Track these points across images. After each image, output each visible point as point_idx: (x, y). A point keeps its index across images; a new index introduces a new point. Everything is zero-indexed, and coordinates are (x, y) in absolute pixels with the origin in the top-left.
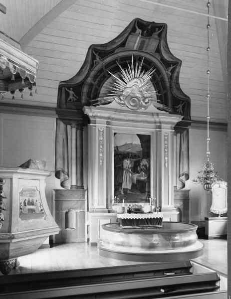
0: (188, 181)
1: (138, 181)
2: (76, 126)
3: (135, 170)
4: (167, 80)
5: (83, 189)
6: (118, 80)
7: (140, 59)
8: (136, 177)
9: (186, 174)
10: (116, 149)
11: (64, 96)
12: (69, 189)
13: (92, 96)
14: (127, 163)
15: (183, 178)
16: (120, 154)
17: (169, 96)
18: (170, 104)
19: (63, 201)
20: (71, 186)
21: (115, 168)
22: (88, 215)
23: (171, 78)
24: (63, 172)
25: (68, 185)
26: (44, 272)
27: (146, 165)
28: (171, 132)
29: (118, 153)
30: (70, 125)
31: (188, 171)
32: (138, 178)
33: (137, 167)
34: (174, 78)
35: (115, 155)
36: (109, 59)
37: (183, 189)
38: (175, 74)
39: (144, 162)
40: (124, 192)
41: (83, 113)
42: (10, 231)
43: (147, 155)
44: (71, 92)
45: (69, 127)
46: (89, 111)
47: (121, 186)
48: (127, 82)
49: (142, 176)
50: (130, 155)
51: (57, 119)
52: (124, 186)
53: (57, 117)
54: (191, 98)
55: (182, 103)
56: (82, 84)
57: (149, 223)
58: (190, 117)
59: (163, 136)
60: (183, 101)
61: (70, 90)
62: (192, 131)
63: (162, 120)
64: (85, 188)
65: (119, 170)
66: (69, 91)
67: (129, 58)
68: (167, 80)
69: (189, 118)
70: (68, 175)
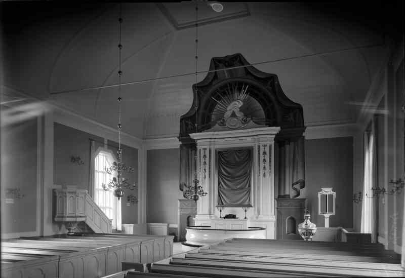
7: (246, 84)
15: (297, 186)
24: (185, 185)
36: (211, 91)
37: (298, 198)
42: (63, 214)
67: (225, 86)
69: (302, 125)
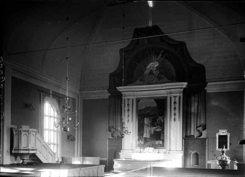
12: (116, 138)
15: (200, 129)
22: (54, 141)
24: (113, 127)
26: (56, 167)
32: (155, 130)
47: (143, 136)
52: (145, 136)
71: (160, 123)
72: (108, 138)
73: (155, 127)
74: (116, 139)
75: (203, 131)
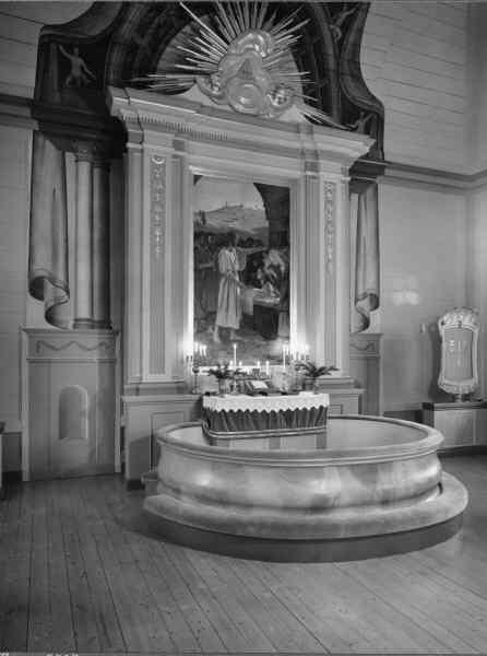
0: (376, 311)
1: (257, 307)
2: (90, 156)
3: (249, 277)
4: (330, 51)
5: (111, 328)
6: (206, 31)
8: (252, 295)
9: (371, 295)
10: (199, 218)
11: (54, 68)
13: (136, 65)
14: (230, 260)
15: (365, 304)
16: (210, 234)
17: (334, 93)
18: (335, 112)
19: (49, 362)
20: (76, 320)
21: (196, 270)
23: (340, 45)
24: (53, 281)
25: (66, 315)
27: (279, 266)
28: (343, 182)
29: (206, 231)
30: (74, 151)
31: (375, 286)
33: (256, 271)
34: (349, 47)
35: (197, 236)
38: (352, 38)
39: (274, 257)
40: (221, 336)
41: (107, 110)
43: (281, 240)
44: (77, 61)
45: (70, 157)
46: (127, 105)
47: (214, 320)
48: (229, 39)
49: (269, 295)
50: (238, 237)
51: (35, 132)
52: (220, 321)
53: (35, 125)
54: (386, 106)
55: (365, 116)
56: (107, 40)
57: (261, 424)
58: (383, 155)
59: (322, 188)
60: (367, 113)
61: (72, 53)
62: (385, 189)
63: (321, 146)
64: (115, 327)
65: (207, 279)
66: (69, 56)
68: (330, 51)
70: (68, 292)
71: (275, 275)
72: (25, 330)
73: (256, 286)
74: (70, 332)
75: (371, 310)
